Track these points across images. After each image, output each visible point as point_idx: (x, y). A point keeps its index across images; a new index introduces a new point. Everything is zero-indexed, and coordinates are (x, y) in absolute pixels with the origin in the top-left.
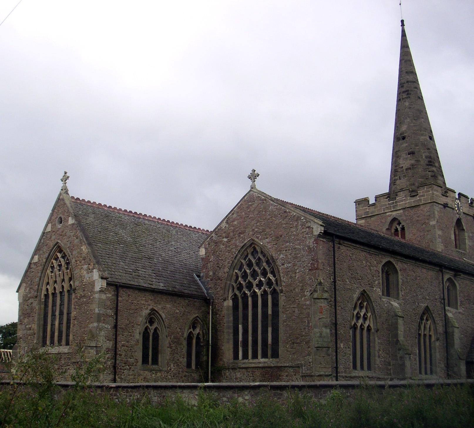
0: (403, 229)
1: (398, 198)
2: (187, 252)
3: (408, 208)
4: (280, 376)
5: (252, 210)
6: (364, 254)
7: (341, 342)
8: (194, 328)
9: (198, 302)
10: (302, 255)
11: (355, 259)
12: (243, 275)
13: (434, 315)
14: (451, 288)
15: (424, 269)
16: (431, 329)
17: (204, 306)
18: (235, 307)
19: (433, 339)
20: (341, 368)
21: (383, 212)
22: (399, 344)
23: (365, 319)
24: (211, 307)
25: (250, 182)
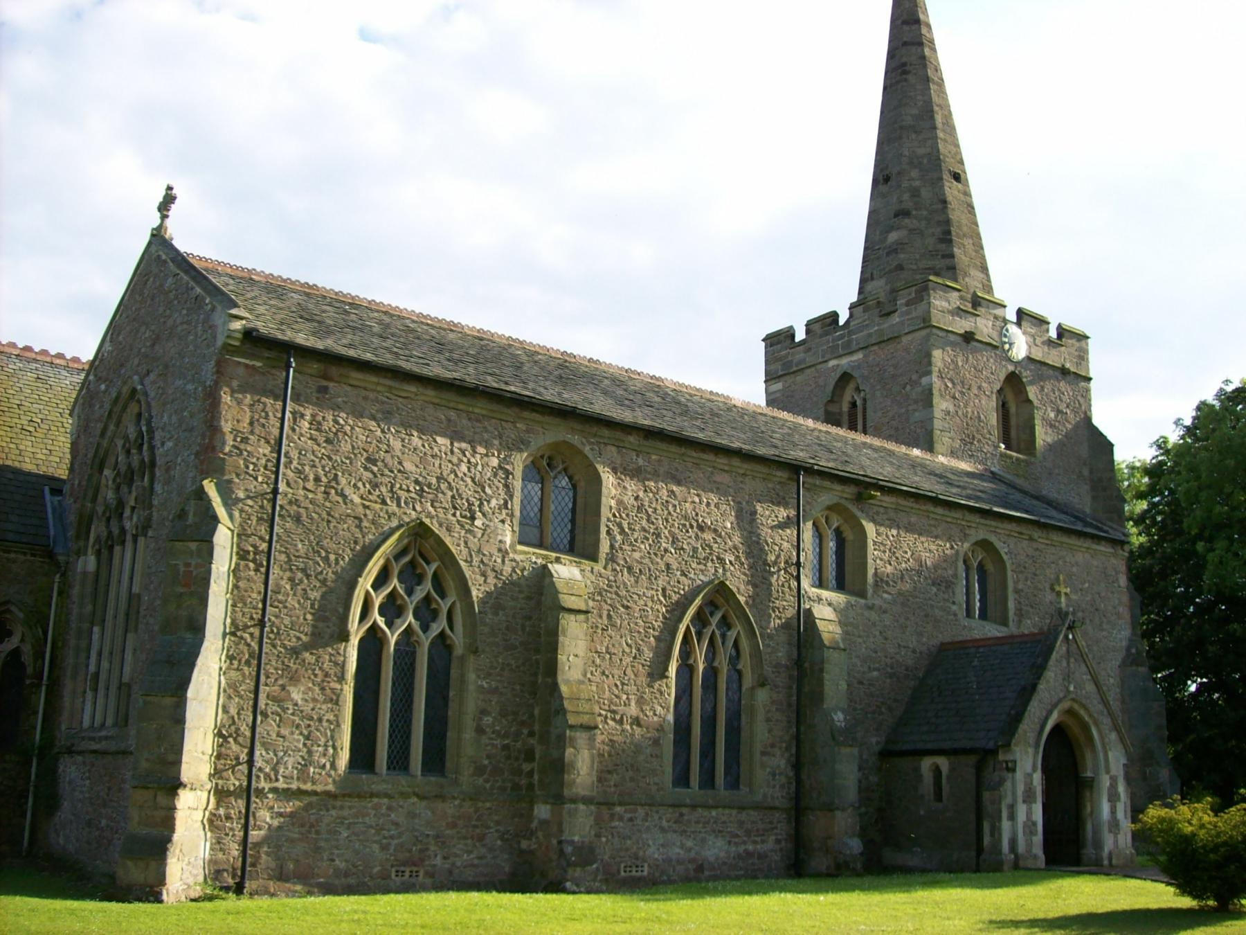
1: (856, 322)
16: (741, 648)
21: (820, 360)
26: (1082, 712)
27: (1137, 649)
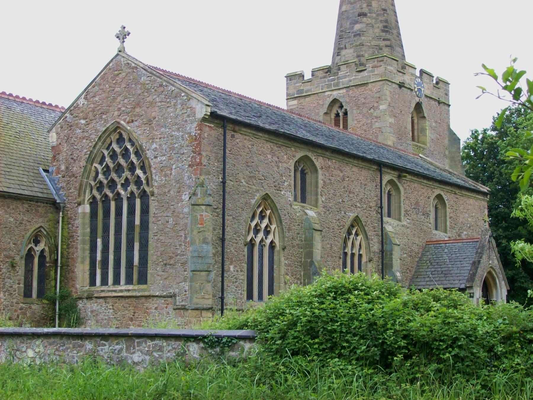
0: (346, 113)
1: (342, 73)
2: (33, 137)
3: (352, 86)
4: (147, 308)
5: (118, 82)
6: (268, 145)
7: (231, 263)
8: (37, 242)
9: (43, 207)
10: (181, 146)
11: (256, 152)
12: (105, 171)
13: (366, 228)
14: (393, 193)
15: (356, 168)
17: (51, 213)
18: (94, 214)
19: (364, 259)
20: (229, 299)
21: (321, 91)
22: (313, 266)
23: (267, 232)
24: (61, 213)
25: (117, 43)
26: (494, 273)
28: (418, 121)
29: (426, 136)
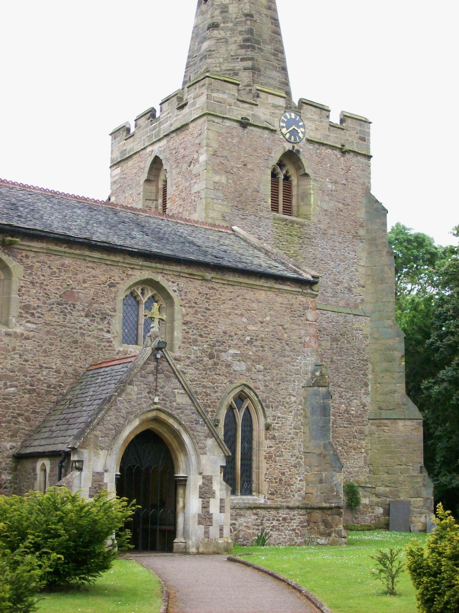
26: (171, 421)
27: (321, 372)
28: (298, 183)
29: (310, 205)
